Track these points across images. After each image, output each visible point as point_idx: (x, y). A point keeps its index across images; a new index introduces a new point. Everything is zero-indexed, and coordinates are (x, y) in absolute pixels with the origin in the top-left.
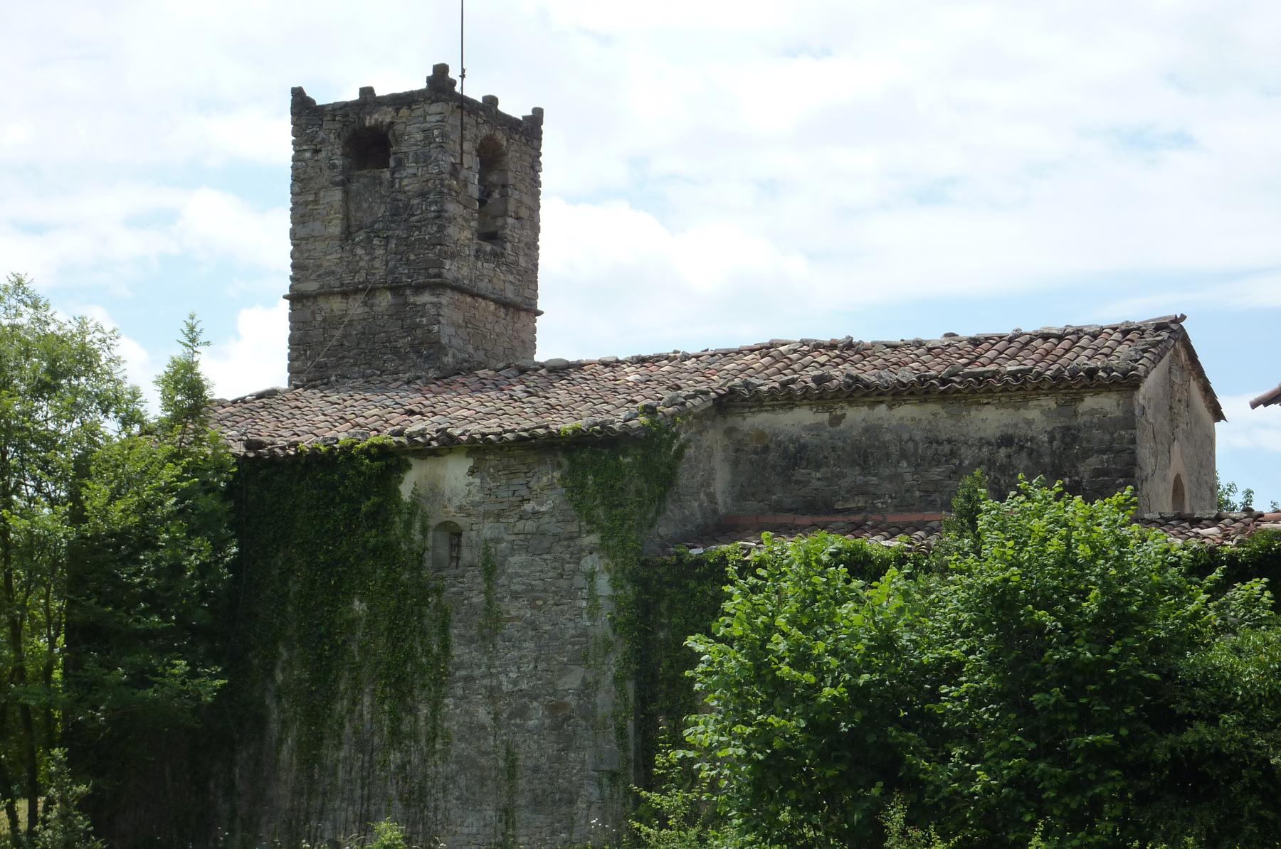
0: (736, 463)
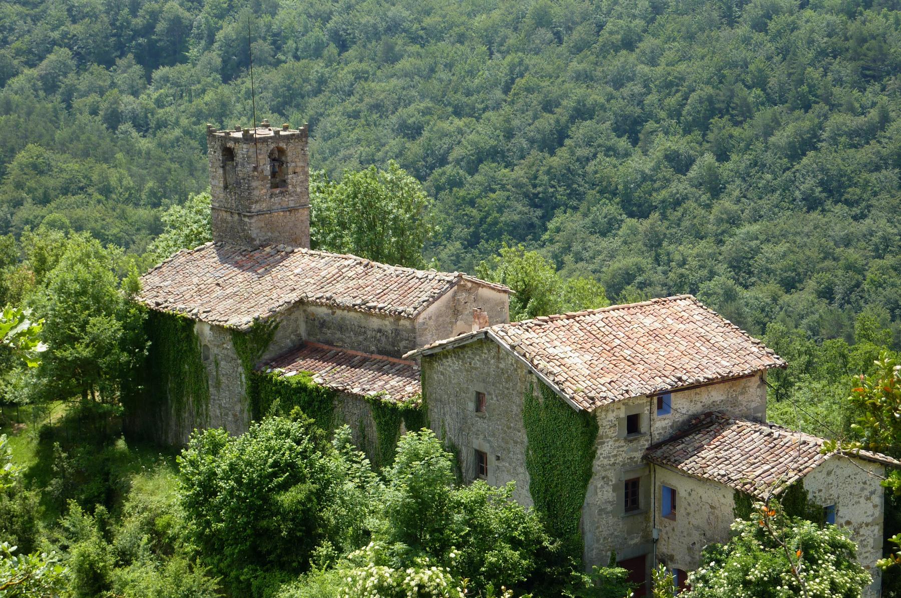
0: (306, 322)
